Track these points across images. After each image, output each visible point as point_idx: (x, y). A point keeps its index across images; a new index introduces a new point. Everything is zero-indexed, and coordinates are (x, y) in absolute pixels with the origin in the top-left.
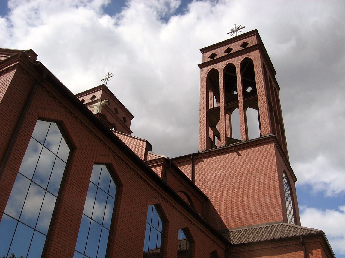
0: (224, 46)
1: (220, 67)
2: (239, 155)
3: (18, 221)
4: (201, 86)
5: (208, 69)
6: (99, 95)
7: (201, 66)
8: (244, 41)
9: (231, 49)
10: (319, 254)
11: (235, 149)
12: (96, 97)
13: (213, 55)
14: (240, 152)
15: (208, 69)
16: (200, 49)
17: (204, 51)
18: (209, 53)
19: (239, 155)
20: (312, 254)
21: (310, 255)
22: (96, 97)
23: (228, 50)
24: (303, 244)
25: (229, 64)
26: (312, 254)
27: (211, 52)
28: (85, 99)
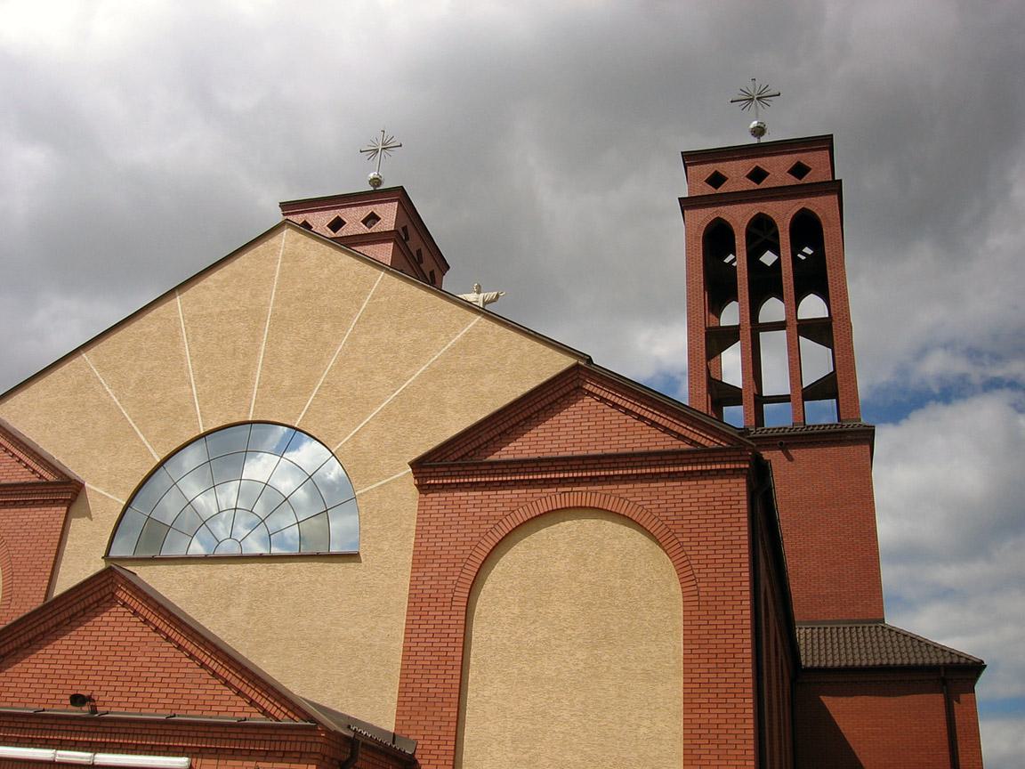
0: (748, 157)
1: (739, 217)
2: (790, 459)
3: (298, 523)
4: (689, 259)
5: (706, 215)
6: (388, 215)
7: (686, 204)
8: (716, 169)
9: (806, 170)
10: (745, 622)
11: (781, 444)
12: (378, 219)
13: (717, 180)
14: (792, 452)
15: (706, 215)
16: (682, 153)
17: (691, 158)
18: (708, 169)
19: (790, 459)
20: (958, 701)
21: (955, 702)
22: (378, 219)
23: (757, 175)
24: (944, 682)
25: (803, 210)
26: (958, 701)
27: (711, 165)
28: (343, 218)
